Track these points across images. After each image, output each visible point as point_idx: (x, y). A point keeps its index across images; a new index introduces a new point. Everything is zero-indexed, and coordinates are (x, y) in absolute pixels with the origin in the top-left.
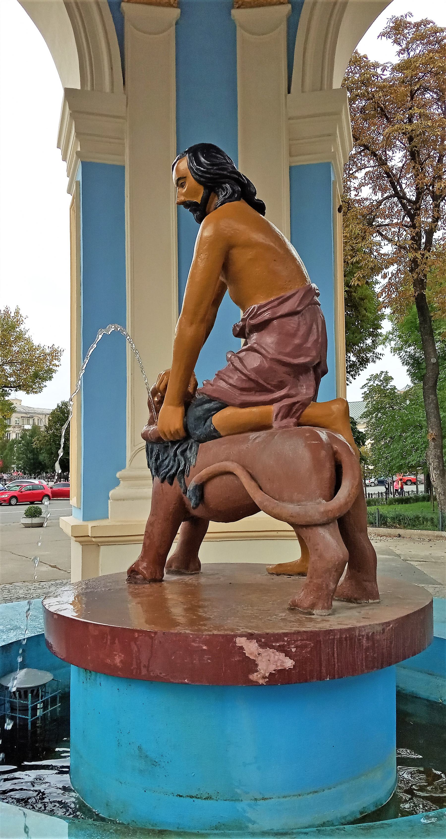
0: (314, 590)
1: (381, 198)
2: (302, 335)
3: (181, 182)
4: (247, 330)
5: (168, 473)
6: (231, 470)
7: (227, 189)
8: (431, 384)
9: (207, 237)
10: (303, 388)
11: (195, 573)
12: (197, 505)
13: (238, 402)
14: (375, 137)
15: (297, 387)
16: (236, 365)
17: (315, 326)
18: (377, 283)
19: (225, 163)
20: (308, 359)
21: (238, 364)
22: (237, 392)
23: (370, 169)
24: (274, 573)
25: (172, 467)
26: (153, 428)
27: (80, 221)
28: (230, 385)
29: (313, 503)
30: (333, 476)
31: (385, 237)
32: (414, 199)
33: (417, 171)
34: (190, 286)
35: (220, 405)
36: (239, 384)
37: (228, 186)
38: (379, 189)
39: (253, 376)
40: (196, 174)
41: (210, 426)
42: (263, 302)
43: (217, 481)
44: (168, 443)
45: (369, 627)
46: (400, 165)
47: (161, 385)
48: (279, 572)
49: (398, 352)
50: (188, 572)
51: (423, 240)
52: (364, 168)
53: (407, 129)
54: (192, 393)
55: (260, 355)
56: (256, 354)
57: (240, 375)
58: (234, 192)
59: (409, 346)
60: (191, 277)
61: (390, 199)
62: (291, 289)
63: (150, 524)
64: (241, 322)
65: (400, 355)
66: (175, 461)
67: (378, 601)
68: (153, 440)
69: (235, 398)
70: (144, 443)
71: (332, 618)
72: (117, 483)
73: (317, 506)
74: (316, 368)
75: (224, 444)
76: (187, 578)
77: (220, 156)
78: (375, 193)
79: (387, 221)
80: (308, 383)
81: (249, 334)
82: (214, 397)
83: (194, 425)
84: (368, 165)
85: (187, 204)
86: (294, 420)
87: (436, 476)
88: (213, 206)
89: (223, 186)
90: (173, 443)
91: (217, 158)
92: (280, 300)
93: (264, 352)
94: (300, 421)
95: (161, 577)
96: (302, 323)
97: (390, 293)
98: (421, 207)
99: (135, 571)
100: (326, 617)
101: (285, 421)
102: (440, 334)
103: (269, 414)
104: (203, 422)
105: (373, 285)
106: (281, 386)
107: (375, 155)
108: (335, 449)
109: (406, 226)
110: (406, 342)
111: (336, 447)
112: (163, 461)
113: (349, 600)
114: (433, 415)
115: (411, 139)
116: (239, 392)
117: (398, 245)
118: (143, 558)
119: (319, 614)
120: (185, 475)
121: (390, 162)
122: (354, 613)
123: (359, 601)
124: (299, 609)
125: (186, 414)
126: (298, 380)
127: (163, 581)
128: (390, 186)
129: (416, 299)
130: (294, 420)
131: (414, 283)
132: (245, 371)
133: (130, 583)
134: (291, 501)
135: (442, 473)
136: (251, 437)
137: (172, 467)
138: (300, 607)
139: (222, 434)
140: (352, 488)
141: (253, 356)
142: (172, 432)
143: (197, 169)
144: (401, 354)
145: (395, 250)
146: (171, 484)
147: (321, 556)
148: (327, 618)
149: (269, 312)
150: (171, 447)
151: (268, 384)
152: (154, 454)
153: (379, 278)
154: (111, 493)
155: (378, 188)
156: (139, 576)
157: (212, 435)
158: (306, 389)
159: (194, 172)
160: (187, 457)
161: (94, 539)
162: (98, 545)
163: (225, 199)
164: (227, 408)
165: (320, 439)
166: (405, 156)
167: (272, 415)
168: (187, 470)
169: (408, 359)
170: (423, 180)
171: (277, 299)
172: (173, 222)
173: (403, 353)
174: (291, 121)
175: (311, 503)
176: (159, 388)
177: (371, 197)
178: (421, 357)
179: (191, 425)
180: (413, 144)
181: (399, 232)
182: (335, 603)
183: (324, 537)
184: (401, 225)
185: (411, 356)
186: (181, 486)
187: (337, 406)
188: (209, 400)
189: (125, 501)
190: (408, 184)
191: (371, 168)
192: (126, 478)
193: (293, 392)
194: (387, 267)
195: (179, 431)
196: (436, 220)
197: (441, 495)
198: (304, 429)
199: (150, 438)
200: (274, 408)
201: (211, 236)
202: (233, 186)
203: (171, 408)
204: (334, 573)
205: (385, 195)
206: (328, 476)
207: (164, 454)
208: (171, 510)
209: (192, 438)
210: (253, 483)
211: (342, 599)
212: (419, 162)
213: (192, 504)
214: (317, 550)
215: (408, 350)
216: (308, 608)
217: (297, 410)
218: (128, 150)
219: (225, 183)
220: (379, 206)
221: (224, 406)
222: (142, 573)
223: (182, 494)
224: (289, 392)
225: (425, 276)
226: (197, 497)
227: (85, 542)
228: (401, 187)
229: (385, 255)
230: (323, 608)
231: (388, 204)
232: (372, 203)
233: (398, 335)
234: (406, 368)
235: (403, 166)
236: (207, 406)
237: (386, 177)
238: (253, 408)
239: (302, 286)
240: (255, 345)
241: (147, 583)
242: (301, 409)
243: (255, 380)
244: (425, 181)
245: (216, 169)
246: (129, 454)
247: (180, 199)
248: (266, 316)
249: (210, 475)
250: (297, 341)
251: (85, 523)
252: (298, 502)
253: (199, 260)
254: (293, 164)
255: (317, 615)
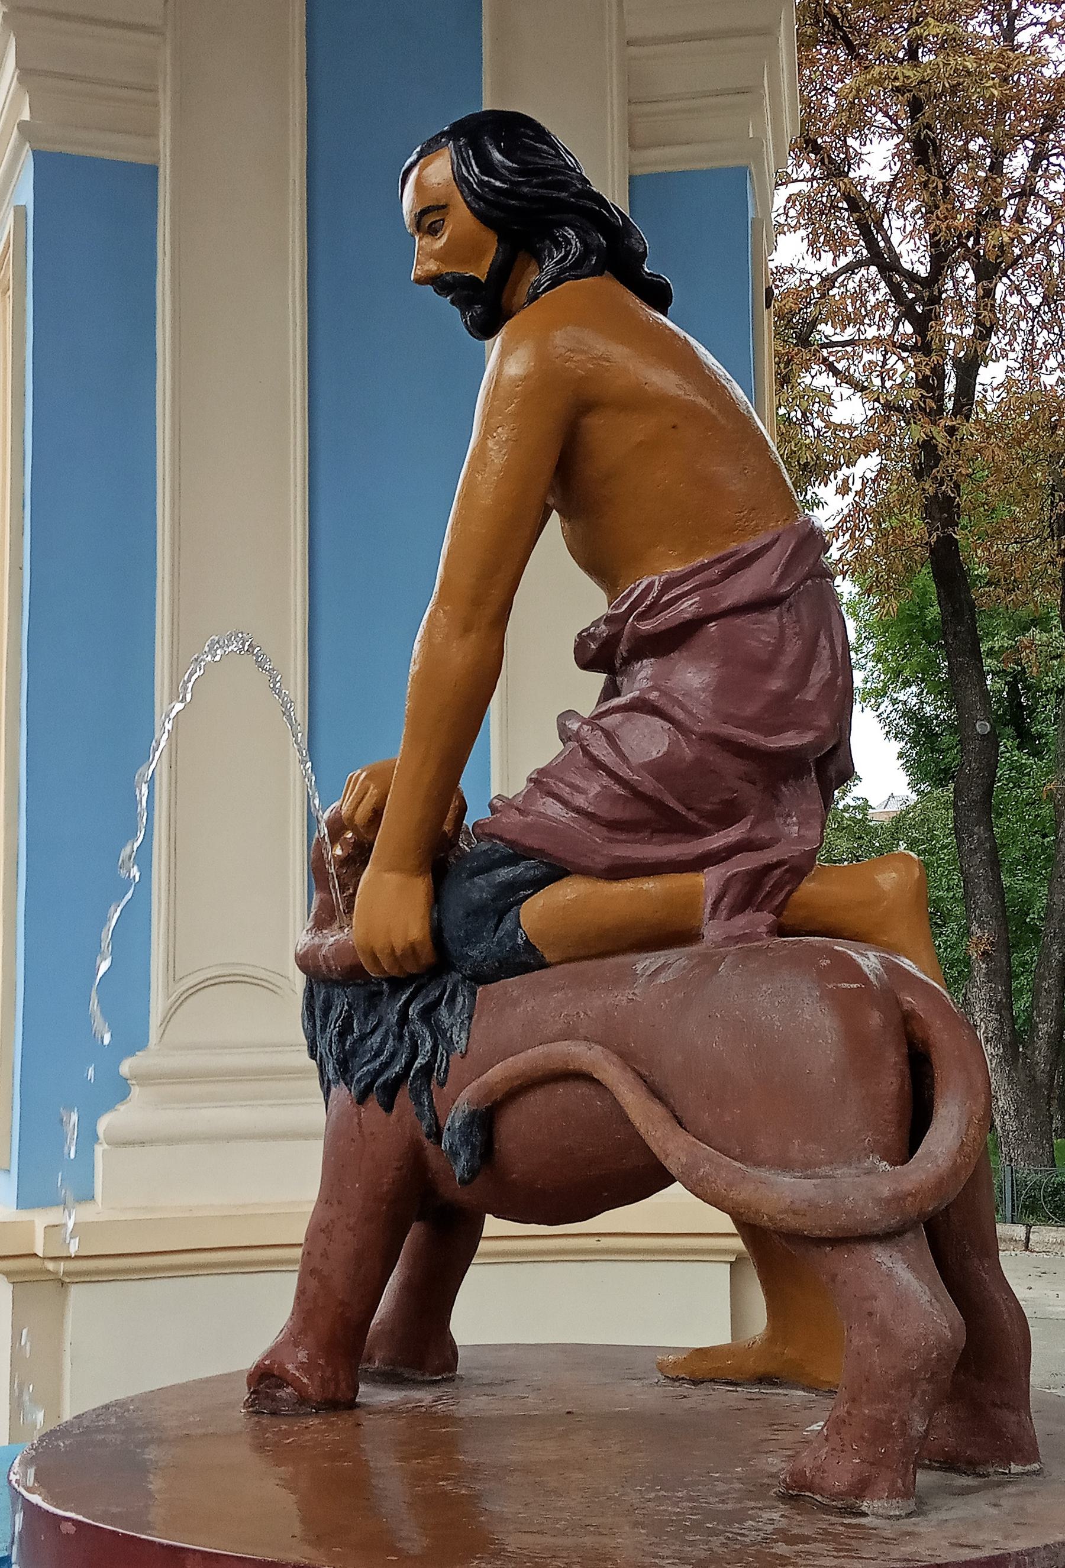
0: (862, 1438)
1: (832, 270)
2: (792, 666)
3: (428, 220)
4: (623, 648)
5: (378, 1073)
6: (586, 1068)
7: (568, 242)
8: (976, 793)
9: (515, 381)
10: (789, 821)
11: (443, 1380)
12: (473, 1172)
13: (601, 862)
14: (814, 98)
15: (773, 820)
16: (596, 753)
17: (823, 641)
18: (818, 503)
19: (561, 166)
20: (808, 737)
21: (601, 750)
22: (597, 836)
23: (804, 186)
24: (683, 1379)
25: (393, 1056)
26: (331, 938)
27: (24, 322)
28: (578, 810)
29: (853, 1172)
30: (906, 1088)
31: (844, 378)
32: (923, 271)
33: (932, 194)
34: (460, 519)
35: (544, 869)
36: (606, 811)
37: (570, 233)
38: (826, 242)
39: (648, 785)
40: (478, 197)
41: (513, 935)
42: (679, 569)
43: (535, 1101)
44: (380, 984)
45: (1043, 1554)
46: (886, 176)
47: (360, 809)
48: (699, 1375)
49: (873, 700)
50: (423, 1375)
51: (950, 387)
52: (785, 184)
53: (908, 77)
54: (450, 835)
55: (667, 725)
56: (657, 722)
57: (606, 781)
58: (587, 250)
59: (907, 684)
60: (466, 495)
61: (856, 271)
62: (755, 531)
63: (319, 1230)
64: (603, 627)
65: (880, 711)
66: (400, 1037)
67: (1036, 1466)
68: (335, 976)
69: (594, 851)
70: (299, 980)
71: (920, 1525)
72: (120, 1090)
73: (864, 1179)
74: (822, 764)
75: (557, 989)
76: (424, 1396)
77: (545, 147)
78: (816, 255)
79: (850, 332)
80: (804, 806)
81: (627, 662)
82: (532, 849)
83: (466, 931)
84: (794, 176)
85: (440, 283)
86: (767, 917)
87: (994, 1062)
88: (524, 290)
89: (553, 233)
90: (397, 984)
91: (537, 152)
92: (729, 562)
93: (680, 715)
94: (781, 919)
95: (351, 1395)
96: (789, 632)
97: (857, 533)
98: (944, 296)
99: (274, 1376)
100: (901, 1521)
101: (741, 921)
102: (991, 653)
103: (691, 902)
104: (492, 924)
105: (807, 511)
106: (726, 816)
107: (816, 149)
108: (906, 1007)
109: (904, 348)
110: (897, 673)
111: (908, 999)
112: (363, 1037)
113: (950, 1464)
114: (984, 885)
115: (915, 107)
116: (605, 832)
117: (882, 401)
118: (294, 1336)
119: (881, 1511)
120: (434, 1082)
121: (857, 169)
122: (979, 1506)
123: (980, 1470)
124: (818, 1497)
125: (437, 898)
126: (775, 797)
127: (357, 1406)
128: (855, 235)
129: (932, 552)
130: (767, 917)
131: (926, 507)
132: (624, 772)
133: (257, 1413)
134: (785, 1165)
135: (1010, 1052)
136: (639, 967)
137: (393, 1056)
138: (821, 1491)
139: (548, 957)
140: (969, 1122)
141: (647, 725)
142: (398, 952)
143: (481, 183)
144: (882, 708)
145: (870, 413)
146: (388, 1107)
147: (884, 1335)
148: (907, 1525)
149: (697, 599)
150: (389, 997)
151: (690, 809)
152: (334, 1014)
153: (826, 492)
154: (104, 1124)
155: (822, 239)
156: (287, 1392)
157: (517, 960)
158: (800, 824)
159: (472, 191)
160: (439, 1027)
161: (50, 1266)
162: (62, 1284)
163: (563, 271)
164: (564, 880)
165: (856, 972)
166: (898, 154)
167: (702, 900)
168: (440, 1067)
169: (902, 722)
170: (950, 221)
171: (719, 560)
172: (295, 331)
173: (886, 706)
174: (633, 50)
175: (845, 1170)
176: (351, 819)
177: (801, 265)
178: (937, 717)
179: (453, 932)
180: (922, 119)
181: (884, 363)
182: (924, 1478)
183: (890, 1275)
184: (890, 345)
185: (909, 715)
186: (420, 1116)
187: (894, 875)
188: (511, 854)
189: (147, 1149)
190: (907, 232)
191: (804, 184)
192: (147, 1079)
193: (763, 833)
194: (851, 463)
195: (418, 948)
196: (985, 332)
197: (1007, 1117)
198: (810, 945)
199: (324, 968)
200: (709, 880)
201: (525, 378)
202: (587, 232)
203: (392, 879)
204: (925, 1386)
205: (843, 261)
206: (894, 1088)
207: (366, 1016)
208: (385, 1188)
209: (456, 970)
210: (658, 1110)
211: (927, 1462)
212: (940, 172)
213: (460, 1168)
214: (870, 1314)
215: (902, 697)
216: (848, 1493)
217: (777, 887)
218: (169, 119)
219: (561, 225)
220: (829, 290)
221: (556, 872)
222: (293, 1382)
223: (424, 1138)
224: (753, 835)
225: (957, 486)
226: (474, 1146)
227: (24, 1272)
228: (887, 240)
229: (841, 426)
230: (893, 1493)
231: (851, 285)
232: (808, 281)
233: (874, 655)
234: (897, 746)
235: (895, 179)
236: (504, 874)
237: (846, 210)
238: (645, 879)
239: (788, 522)
240: (654, 695)
241: (311, 1413)
242: (787, 883)
243: (656, 797)
244: (956, 223)
245: (539, 186)
246: (158, 1005)
247: (426, 268)
248: (688, 607)
249: (516, 1083)
250: (776, 684)
251: (25, 1216)
252: (806, 1167)
253: (490, 443)
254: (638, 171)
255: (877, 1515)
